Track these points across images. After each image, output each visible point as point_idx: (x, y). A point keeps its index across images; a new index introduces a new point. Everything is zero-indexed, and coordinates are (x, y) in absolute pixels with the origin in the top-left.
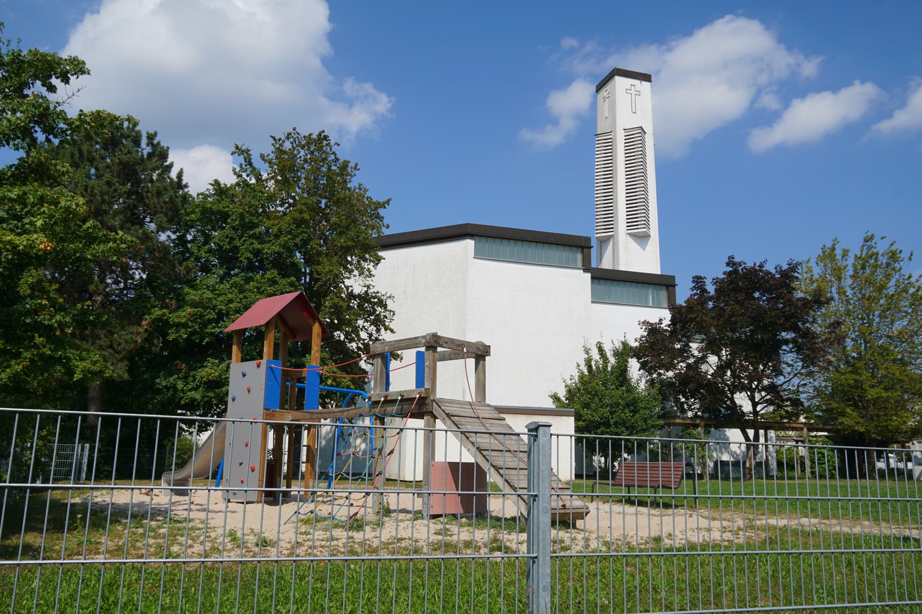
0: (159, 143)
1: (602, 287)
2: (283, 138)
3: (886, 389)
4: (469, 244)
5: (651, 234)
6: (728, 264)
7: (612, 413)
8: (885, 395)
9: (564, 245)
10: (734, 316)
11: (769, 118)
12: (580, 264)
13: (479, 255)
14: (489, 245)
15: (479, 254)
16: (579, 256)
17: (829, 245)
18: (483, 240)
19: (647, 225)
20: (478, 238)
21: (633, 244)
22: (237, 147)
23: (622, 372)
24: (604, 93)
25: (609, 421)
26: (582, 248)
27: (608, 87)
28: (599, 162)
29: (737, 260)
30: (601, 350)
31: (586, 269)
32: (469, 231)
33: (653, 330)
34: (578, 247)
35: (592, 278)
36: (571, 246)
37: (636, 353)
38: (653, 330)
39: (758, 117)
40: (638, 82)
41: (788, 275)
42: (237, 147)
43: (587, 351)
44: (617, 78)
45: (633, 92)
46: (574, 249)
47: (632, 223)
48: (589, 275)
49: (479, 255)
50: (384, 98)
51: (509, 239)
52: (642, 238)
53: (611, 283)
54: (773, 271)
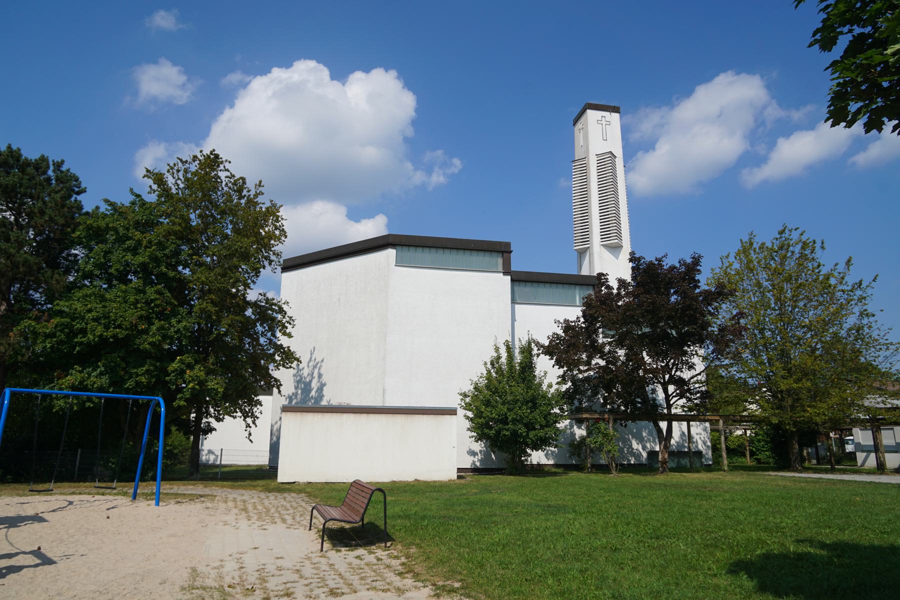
0: (68, 170)
1: (525, 290)
2: (189, 160)
3: (796, 382)
4: (391, 253)
5: (624, 244)
6: (631, 260)
7: (509, 410)
8: (795, 386)
9: (485, 251)
10: (628, 310)
11: (758, 160)
12: (500, 268)
13: (400, 263)
14: (411, 253)
15: (400, 262)
16: (500, 261)
17: (746, 239)
18: (405, 249)
19: (619, 236)
20: (399, 248)
21: (606, 254)
22: (148, 171)
23: (528, 366)
24: (579, 125)
25: (507, 418)
26: (503, 252)
27: (582, 120)
28: (576, 183)
29: (637, 256)
30: (509, 349)
31: (505, 273)
32: (390, 241)
33: (568, 327)
34: (498, 252)
35: (512, 280)
36: (491, 251)
37: (549, 351)
38: (568, 327)
39: (752, 158)
40: (608, 113)
41: (692, 268)
42: (148, 171)
43: (497, 349)
44: (588, 111)
45: (604, 122)
46: (495, 254)
47: (605, 235)
48: (509, 277)
49: (400, 263)
50: (456, 162)
51: (430, 247)
52: (615, 249)
53: (528, 283)
54: (678, 265)
